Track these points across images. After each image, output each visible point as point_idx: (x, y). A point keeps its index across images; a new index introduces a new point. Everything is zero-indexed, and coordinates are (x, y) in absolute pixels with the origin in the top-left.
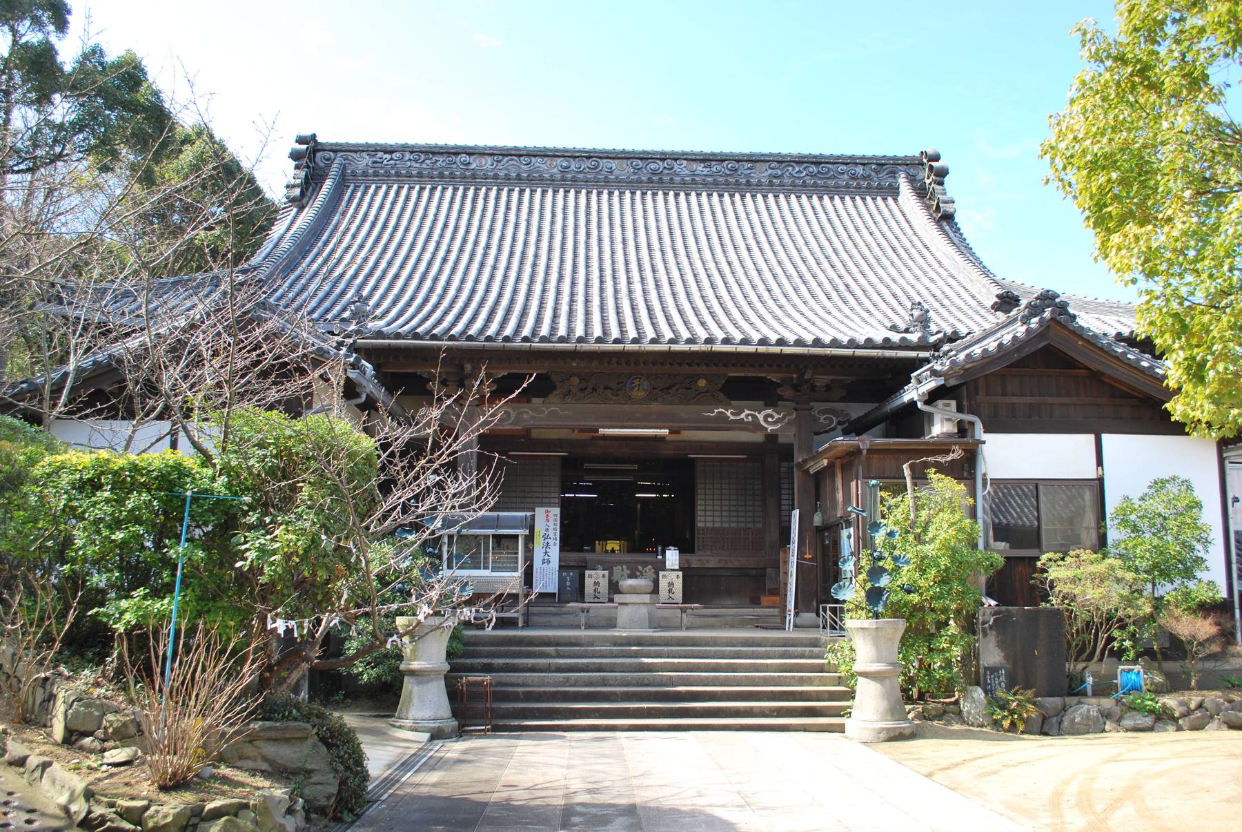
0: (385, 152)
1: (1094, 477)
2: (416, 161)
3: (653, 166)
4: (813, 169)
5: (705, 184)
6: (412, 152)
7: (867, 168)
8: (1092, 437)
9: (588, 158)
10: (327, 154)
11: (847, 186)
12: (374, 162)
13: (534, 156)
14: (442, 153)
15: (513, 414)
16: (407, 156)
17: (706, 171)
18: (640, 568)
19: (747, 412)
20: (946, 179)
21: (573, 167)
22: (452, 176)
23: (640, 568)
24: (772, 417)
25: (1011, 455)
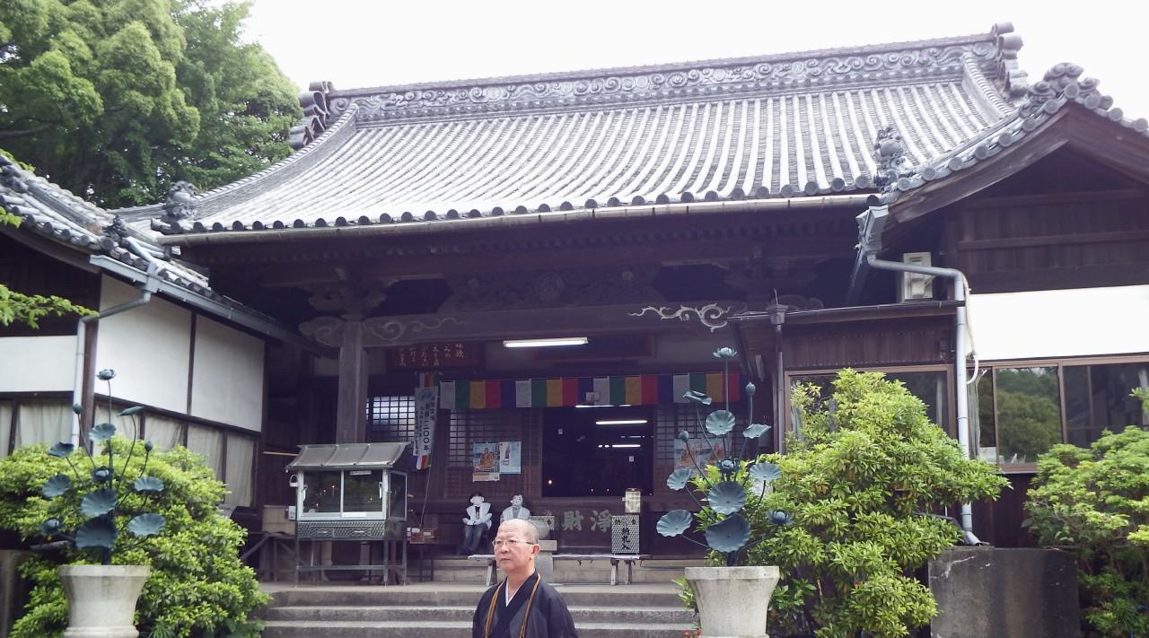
0: (398, 93)
2: (428, 99)
3: (676, 79)
5: (732, 92)
6: (424, 90)
7: (925, 53)
9: (606, 77)
10: (341, 101)
12: (388, 105)
13: (550, 81)
15: (402, 328)
16: (420, 95)
17: (735, 78)
18: (595, 513)
20: (1019, 54)
21: (589, 90)
23: (595, 513)
24: (717, 314)
25: (1010, 327)
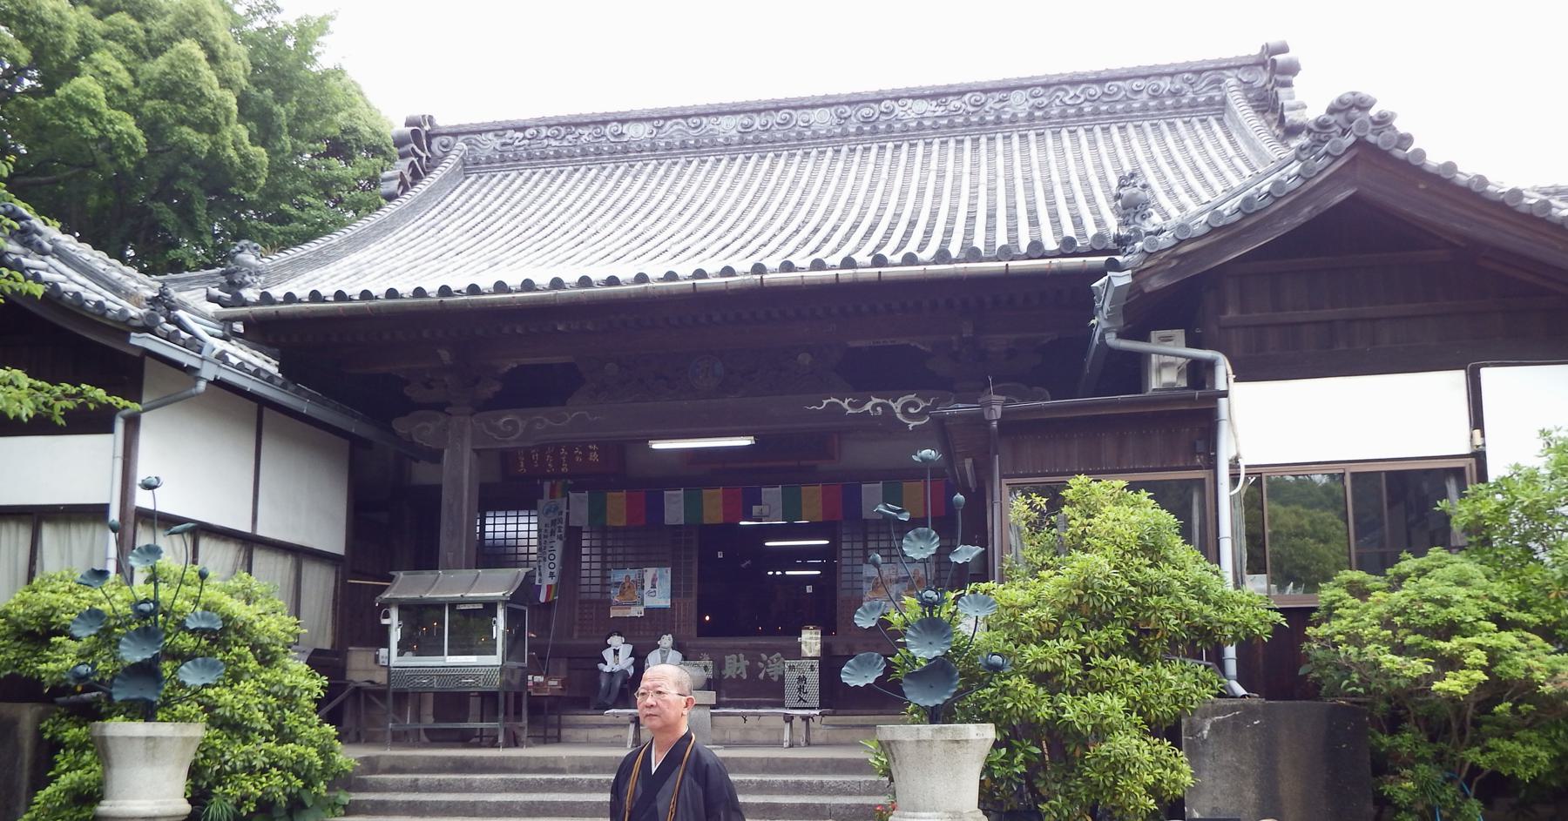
0: (517, 129)
1: (1466, 450)
2: (555, 138)
3: (865, 111)
4: (1095, 90)
5: (936, 128)
6: (549, 126)
7: (1178, 79)
8: (1458, 377)
10: (445, 140)
11: (1145, 108)
12: (504, 144)
13: (707, 115)
14: (586, 124)
15: (522, 424)
16: (544, 131)
17: (940, 111)
19: (875, 400)
21: (757, 125)
22: (598, 152)
24: (916, 406)
25: (1284, 423)
